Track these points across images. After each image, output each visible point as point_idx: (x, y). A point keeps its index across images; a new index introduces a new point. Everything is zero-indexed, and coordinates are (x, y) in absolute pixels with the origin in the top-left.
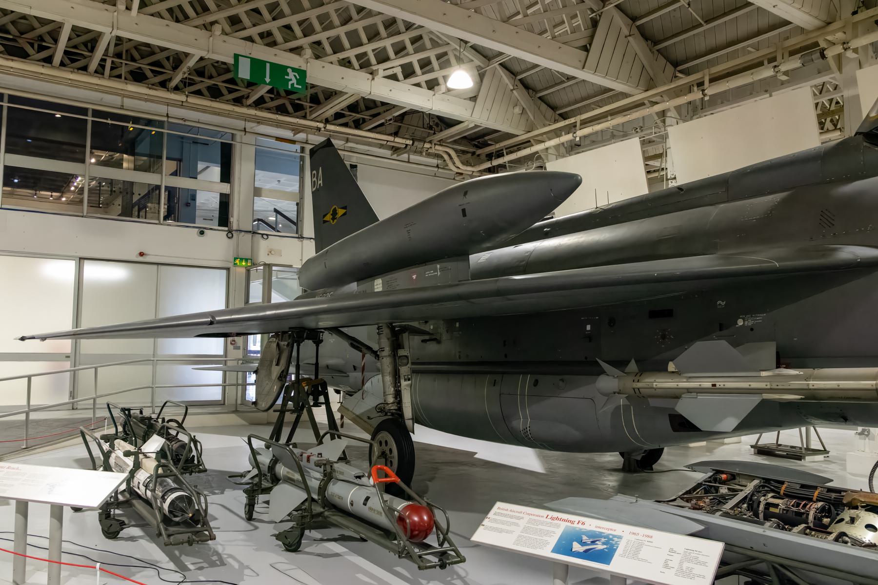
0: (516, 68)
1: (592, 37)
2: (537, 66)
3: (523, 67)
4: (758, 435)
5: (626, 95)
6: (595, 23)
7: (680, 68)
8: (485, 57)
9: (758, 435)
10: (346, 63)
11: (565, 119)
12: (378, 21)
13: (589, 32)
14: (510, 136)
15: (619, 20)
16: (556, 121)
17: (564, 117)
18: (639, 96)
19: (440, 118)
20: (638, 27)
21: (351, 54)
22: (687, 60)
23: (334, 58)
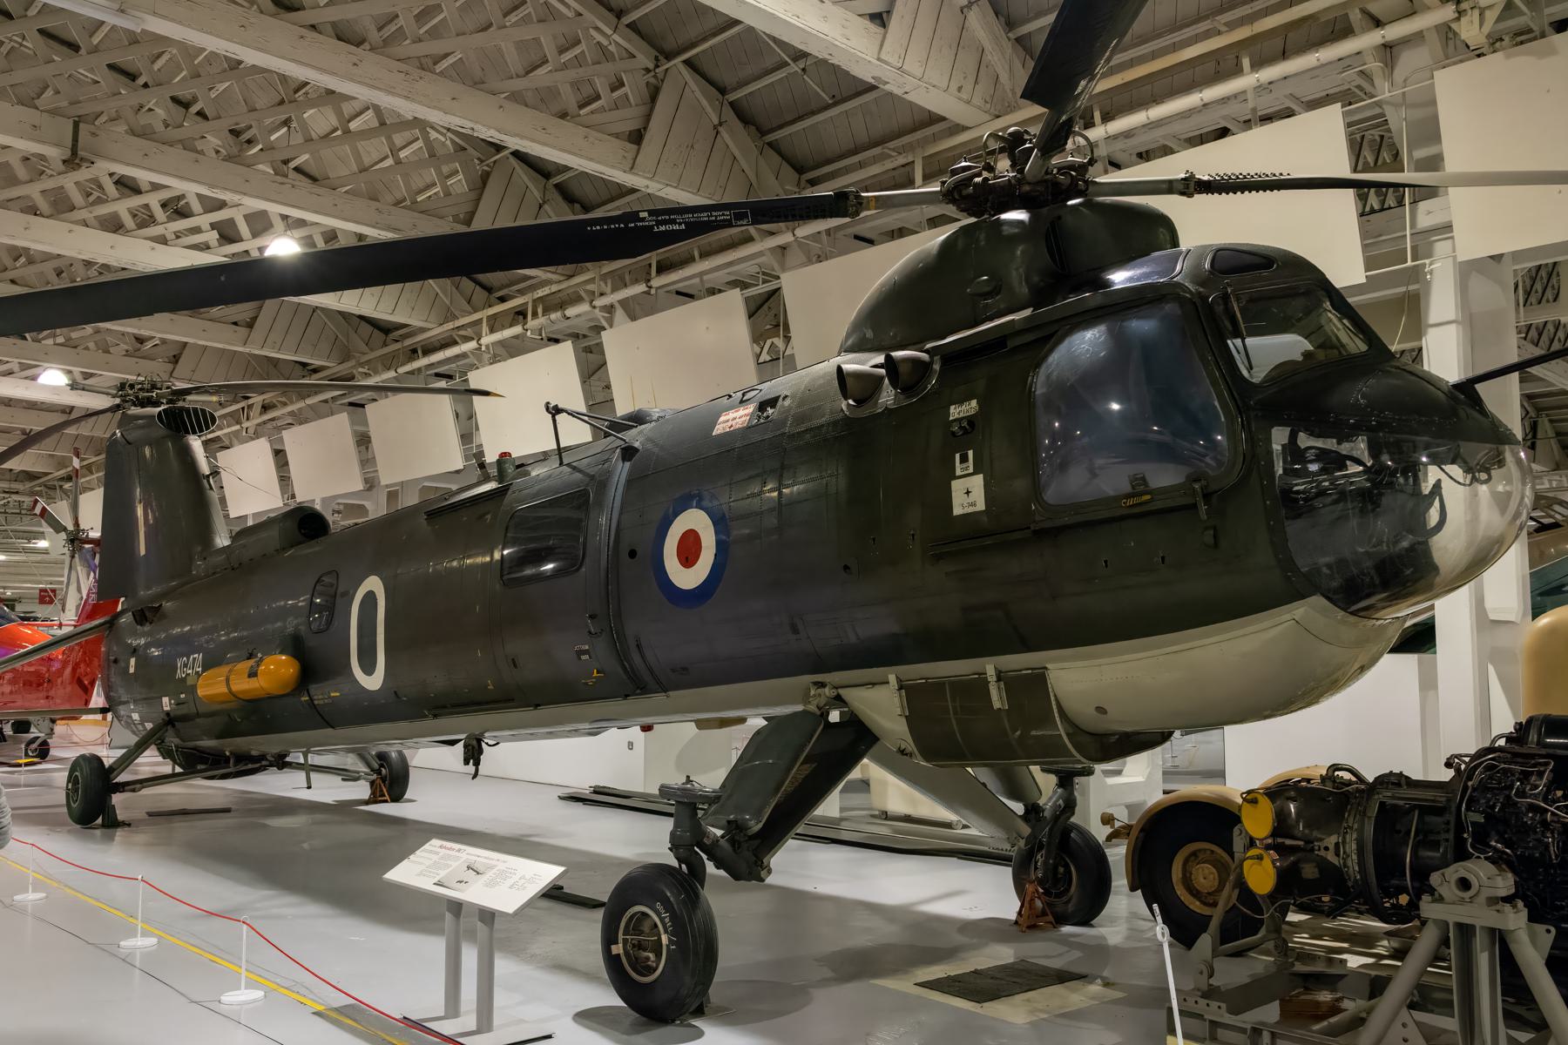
1: (478, 200)
13: (473, 196)
17: (502, 299)
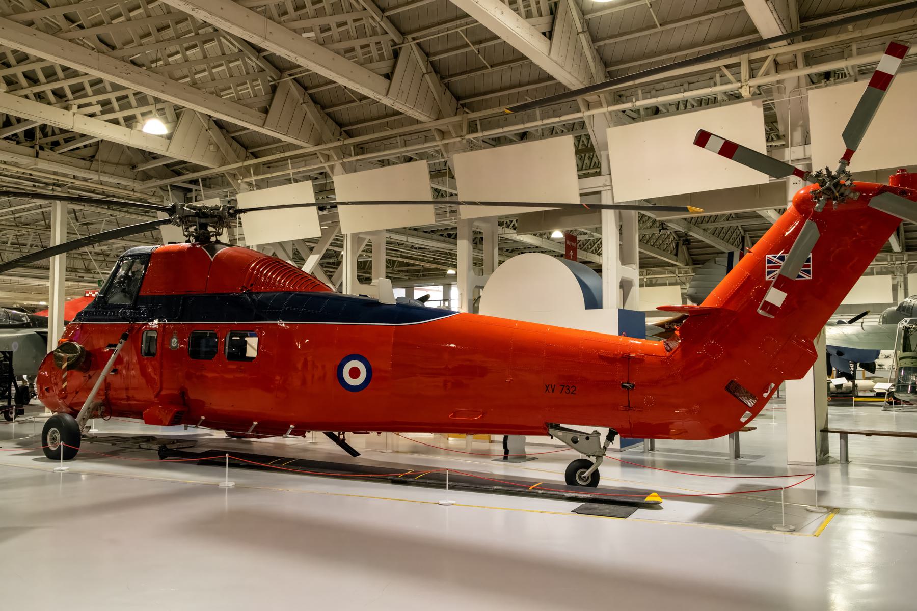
0: (307, 83)
1: (272, 99)
2: (334, 82)
3: (316, 82)
4: (854, 167)
5: (297, 147)
6: (274, 89)
7: (344, 129)
8: (400, 31)
9: (854, 167)
10: (40, 97)
11: (257, 158)
12: (37, 67)
13: (268, 97)
14: (196, 168)
15: (294, 90)
16: (247, 158)
18: (310, 148)
19: (142, 152)
20: (310, 95)
21: (47, 88)
22: (351, 124)
23: (29, 91)
